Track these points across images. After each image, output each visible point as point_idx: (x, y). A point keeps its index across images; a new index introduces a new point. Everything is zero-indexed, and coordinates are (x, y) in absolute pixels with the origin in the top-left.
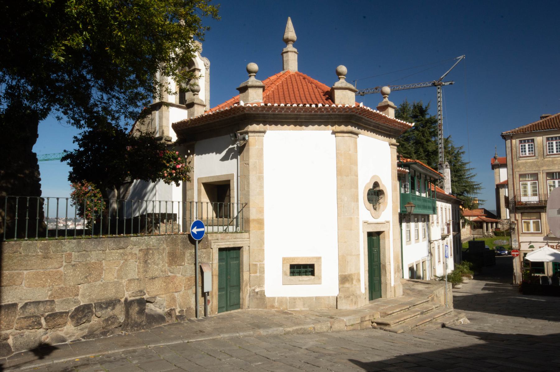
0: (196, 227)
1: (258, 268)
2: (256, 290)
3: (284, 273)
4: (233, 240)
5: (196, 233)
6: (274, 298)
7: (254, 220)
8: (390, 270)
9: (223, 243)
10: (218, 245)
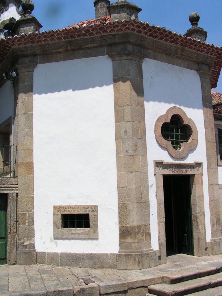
1: (27, 218)
2: (25, 244)
3: (55, 225)
6: (44, 253)
7: (22, 164)
8: (205, 222)
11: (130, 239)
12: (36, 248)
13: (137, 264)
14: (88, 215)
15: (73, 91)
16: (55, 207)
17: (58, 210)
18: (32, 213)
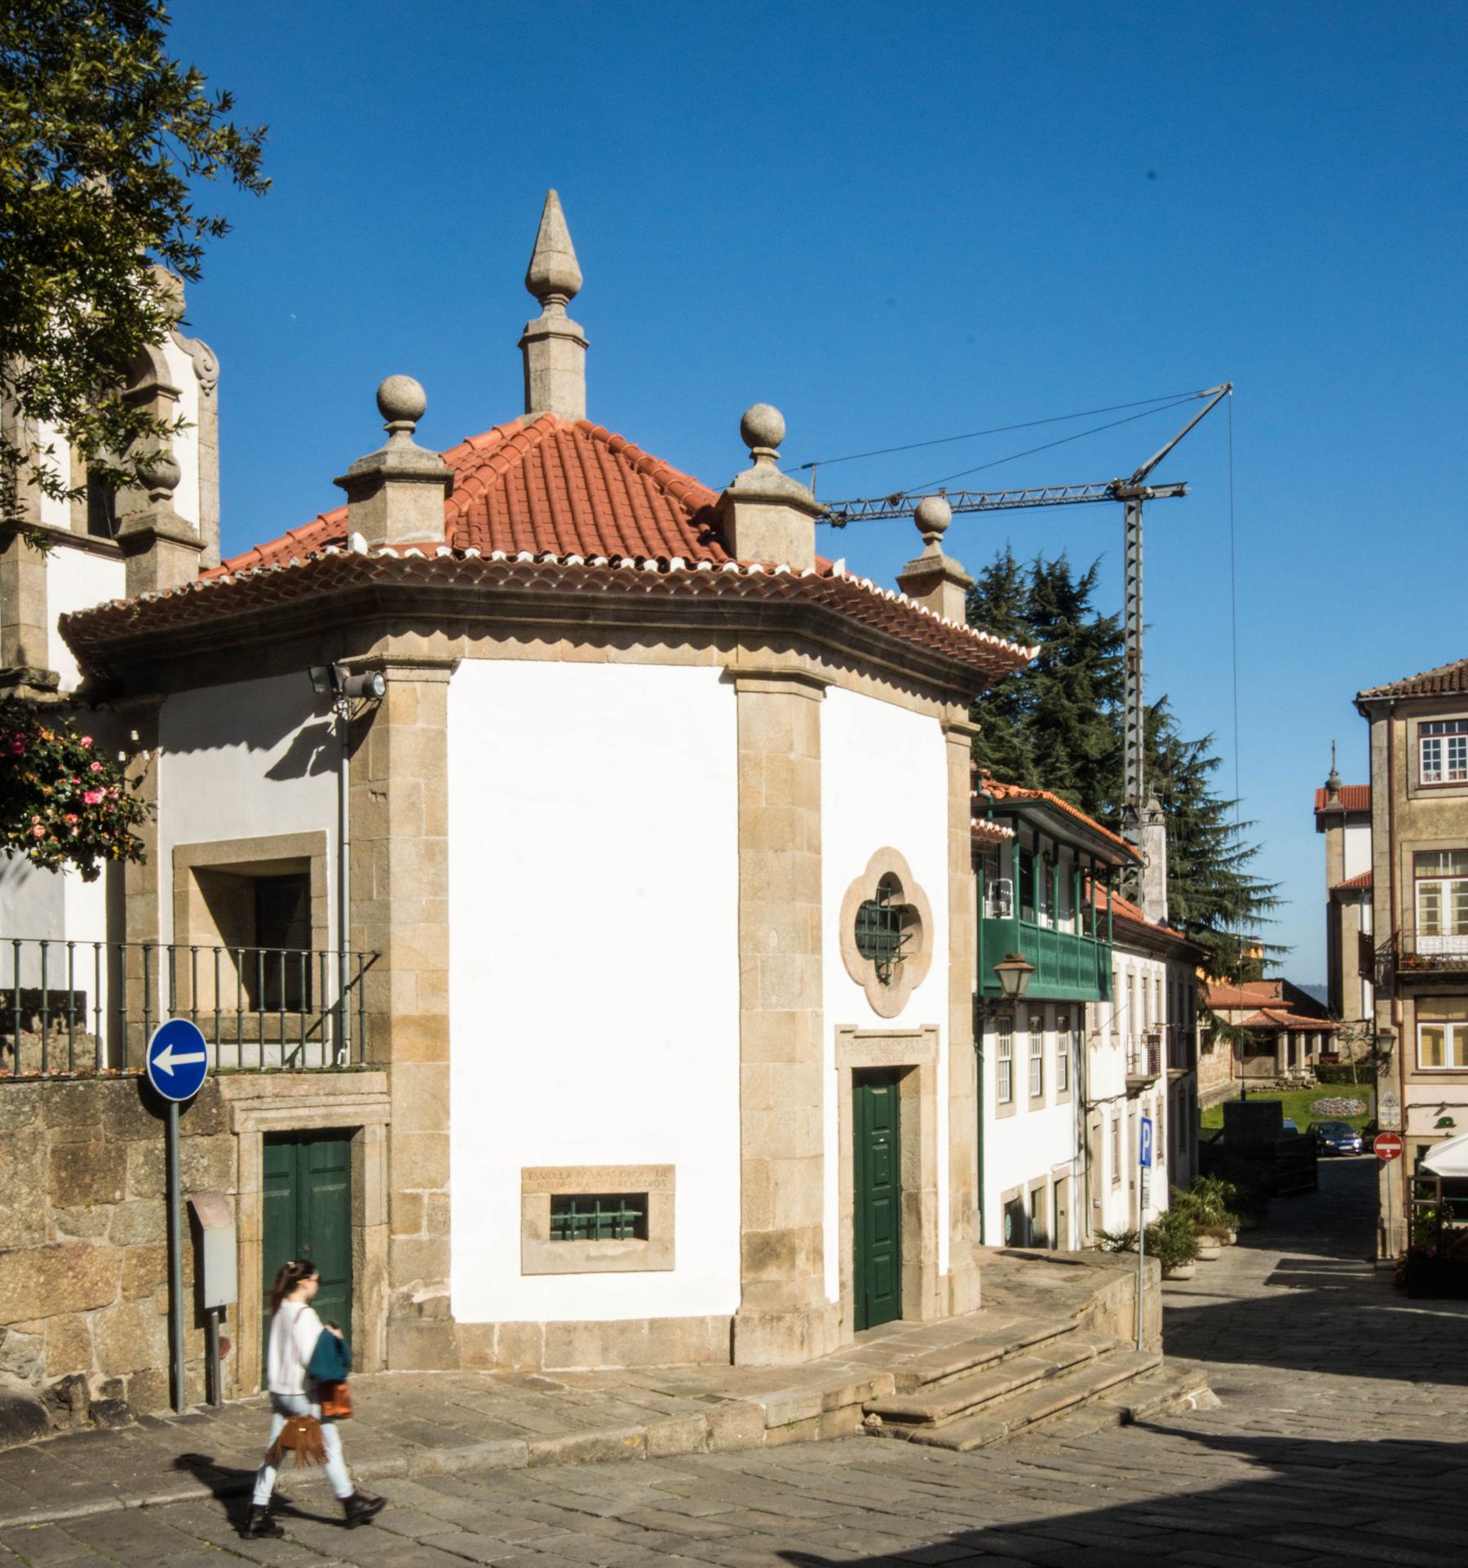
0: (170, 1047)
1: (424, 1212)
3: (529, 1230)
4: (324, 1100)
5: (171, 1072)
7: (407, 1021)
9: (283, 1113)
10: (264, 1120)
11: (775, 1269)
12: (455, 1312)
13: (797, 1344)
15: (251, 748)
16: (528, 1174)
17: (541, 1180)
18: (443, 1194)
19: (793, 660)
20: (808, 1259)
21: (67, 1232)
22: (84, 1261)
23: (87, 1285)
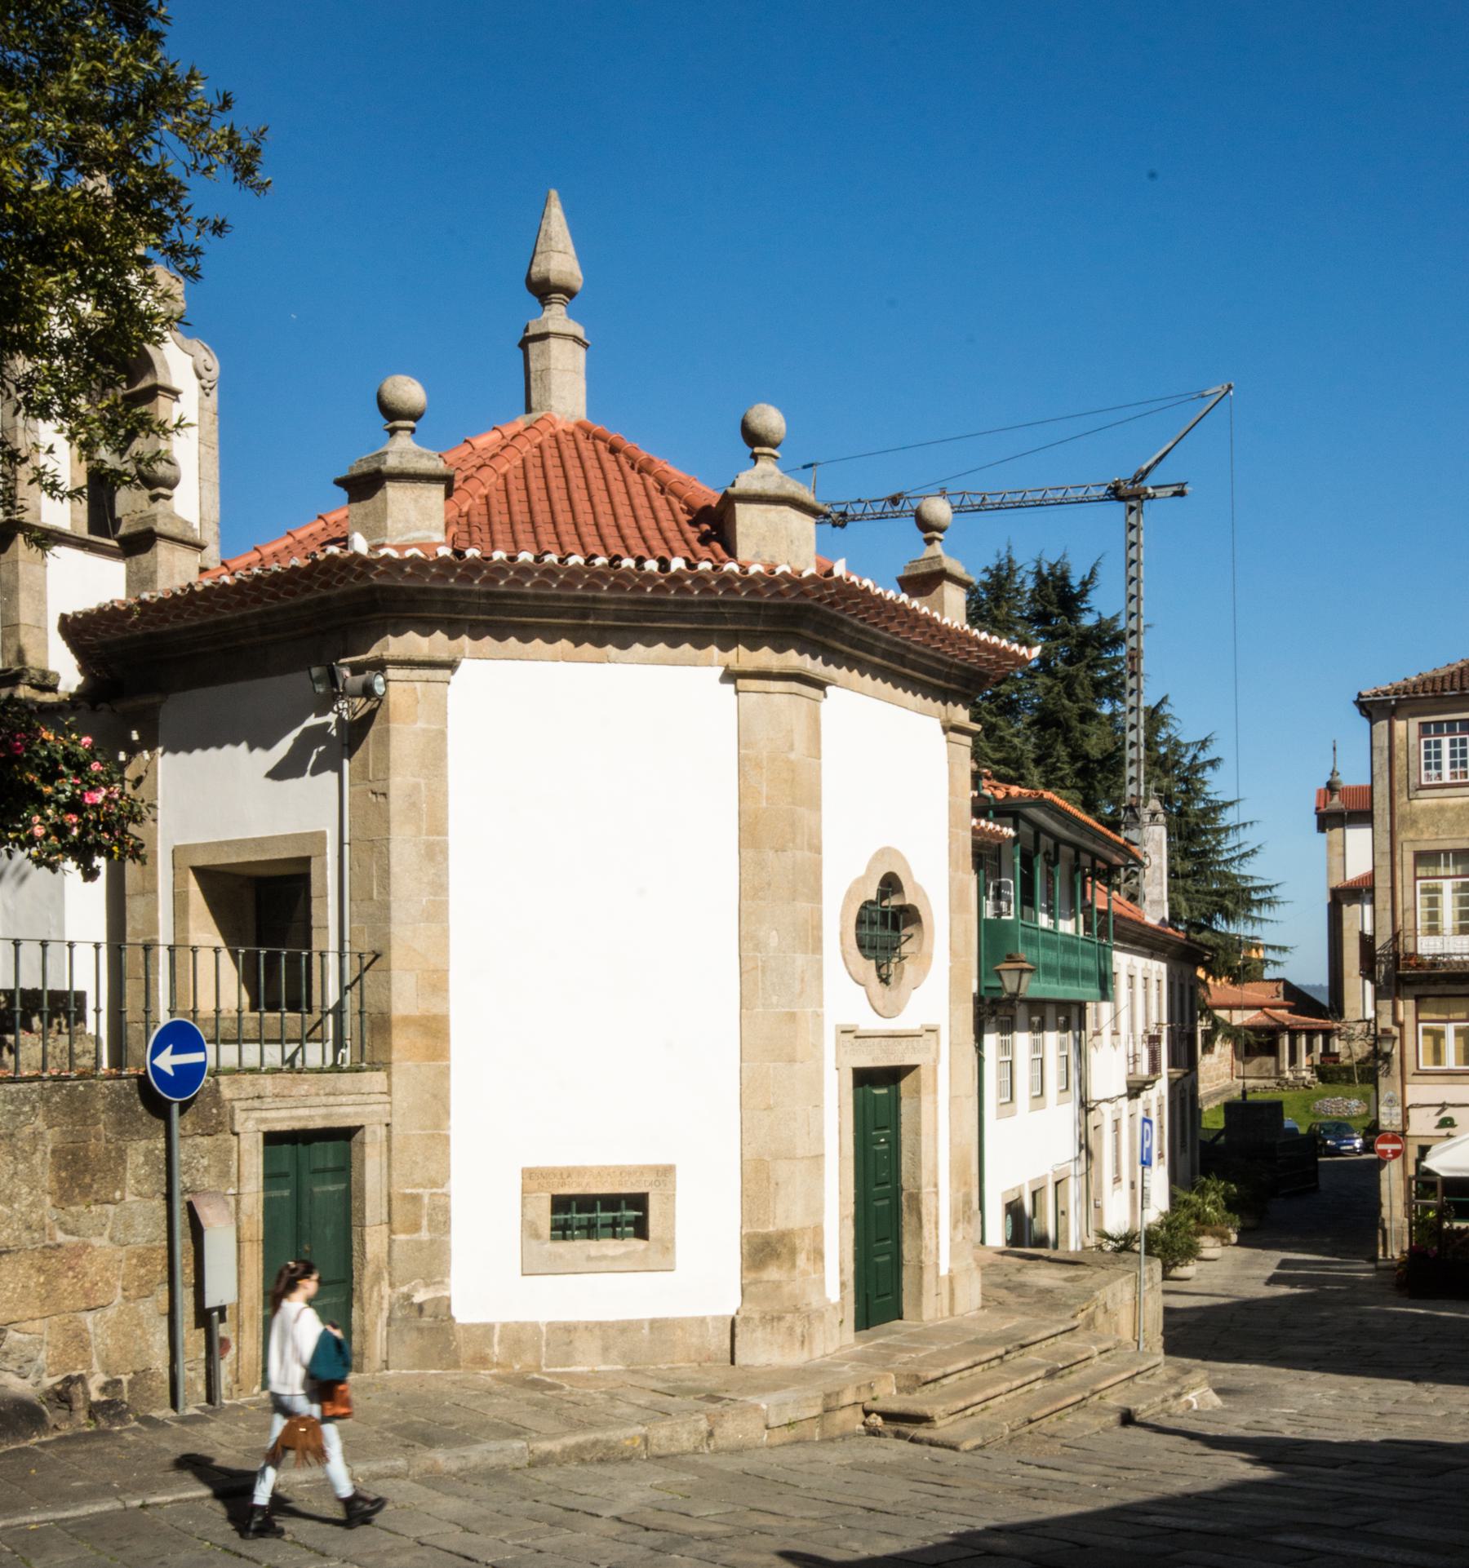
0: (170, 1047)
1: (425, 1212)
2: (418, 1298)
3: (529, 1230)
4: (324, 1100)
7: (407, 1020)
9: (284, 1113)
10: (264, 1120)
12: (455, 1312)
13: (798, 1344)
14: (554, 1198)
16: (529, 1174)
17: (541, 1180)
19: (793, 660)
20: (808, 1259)
21: (67, 1232)
22: (84, 1261)
23: (87, 1285)
